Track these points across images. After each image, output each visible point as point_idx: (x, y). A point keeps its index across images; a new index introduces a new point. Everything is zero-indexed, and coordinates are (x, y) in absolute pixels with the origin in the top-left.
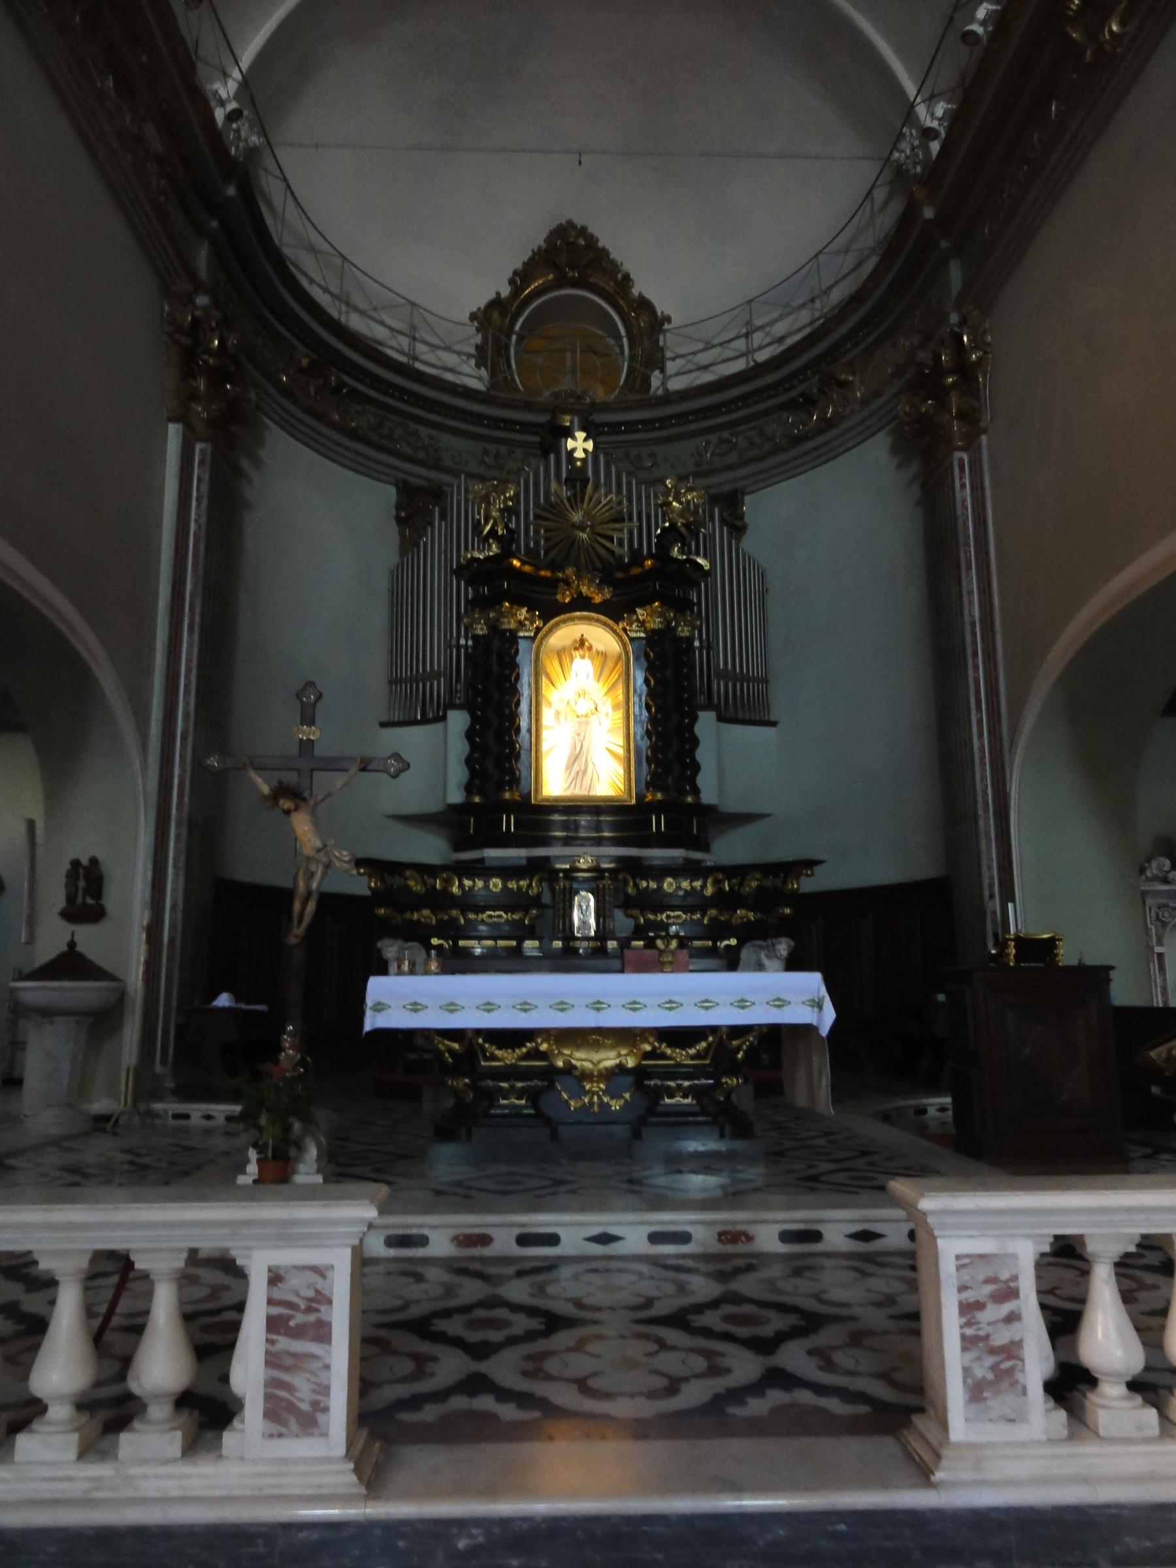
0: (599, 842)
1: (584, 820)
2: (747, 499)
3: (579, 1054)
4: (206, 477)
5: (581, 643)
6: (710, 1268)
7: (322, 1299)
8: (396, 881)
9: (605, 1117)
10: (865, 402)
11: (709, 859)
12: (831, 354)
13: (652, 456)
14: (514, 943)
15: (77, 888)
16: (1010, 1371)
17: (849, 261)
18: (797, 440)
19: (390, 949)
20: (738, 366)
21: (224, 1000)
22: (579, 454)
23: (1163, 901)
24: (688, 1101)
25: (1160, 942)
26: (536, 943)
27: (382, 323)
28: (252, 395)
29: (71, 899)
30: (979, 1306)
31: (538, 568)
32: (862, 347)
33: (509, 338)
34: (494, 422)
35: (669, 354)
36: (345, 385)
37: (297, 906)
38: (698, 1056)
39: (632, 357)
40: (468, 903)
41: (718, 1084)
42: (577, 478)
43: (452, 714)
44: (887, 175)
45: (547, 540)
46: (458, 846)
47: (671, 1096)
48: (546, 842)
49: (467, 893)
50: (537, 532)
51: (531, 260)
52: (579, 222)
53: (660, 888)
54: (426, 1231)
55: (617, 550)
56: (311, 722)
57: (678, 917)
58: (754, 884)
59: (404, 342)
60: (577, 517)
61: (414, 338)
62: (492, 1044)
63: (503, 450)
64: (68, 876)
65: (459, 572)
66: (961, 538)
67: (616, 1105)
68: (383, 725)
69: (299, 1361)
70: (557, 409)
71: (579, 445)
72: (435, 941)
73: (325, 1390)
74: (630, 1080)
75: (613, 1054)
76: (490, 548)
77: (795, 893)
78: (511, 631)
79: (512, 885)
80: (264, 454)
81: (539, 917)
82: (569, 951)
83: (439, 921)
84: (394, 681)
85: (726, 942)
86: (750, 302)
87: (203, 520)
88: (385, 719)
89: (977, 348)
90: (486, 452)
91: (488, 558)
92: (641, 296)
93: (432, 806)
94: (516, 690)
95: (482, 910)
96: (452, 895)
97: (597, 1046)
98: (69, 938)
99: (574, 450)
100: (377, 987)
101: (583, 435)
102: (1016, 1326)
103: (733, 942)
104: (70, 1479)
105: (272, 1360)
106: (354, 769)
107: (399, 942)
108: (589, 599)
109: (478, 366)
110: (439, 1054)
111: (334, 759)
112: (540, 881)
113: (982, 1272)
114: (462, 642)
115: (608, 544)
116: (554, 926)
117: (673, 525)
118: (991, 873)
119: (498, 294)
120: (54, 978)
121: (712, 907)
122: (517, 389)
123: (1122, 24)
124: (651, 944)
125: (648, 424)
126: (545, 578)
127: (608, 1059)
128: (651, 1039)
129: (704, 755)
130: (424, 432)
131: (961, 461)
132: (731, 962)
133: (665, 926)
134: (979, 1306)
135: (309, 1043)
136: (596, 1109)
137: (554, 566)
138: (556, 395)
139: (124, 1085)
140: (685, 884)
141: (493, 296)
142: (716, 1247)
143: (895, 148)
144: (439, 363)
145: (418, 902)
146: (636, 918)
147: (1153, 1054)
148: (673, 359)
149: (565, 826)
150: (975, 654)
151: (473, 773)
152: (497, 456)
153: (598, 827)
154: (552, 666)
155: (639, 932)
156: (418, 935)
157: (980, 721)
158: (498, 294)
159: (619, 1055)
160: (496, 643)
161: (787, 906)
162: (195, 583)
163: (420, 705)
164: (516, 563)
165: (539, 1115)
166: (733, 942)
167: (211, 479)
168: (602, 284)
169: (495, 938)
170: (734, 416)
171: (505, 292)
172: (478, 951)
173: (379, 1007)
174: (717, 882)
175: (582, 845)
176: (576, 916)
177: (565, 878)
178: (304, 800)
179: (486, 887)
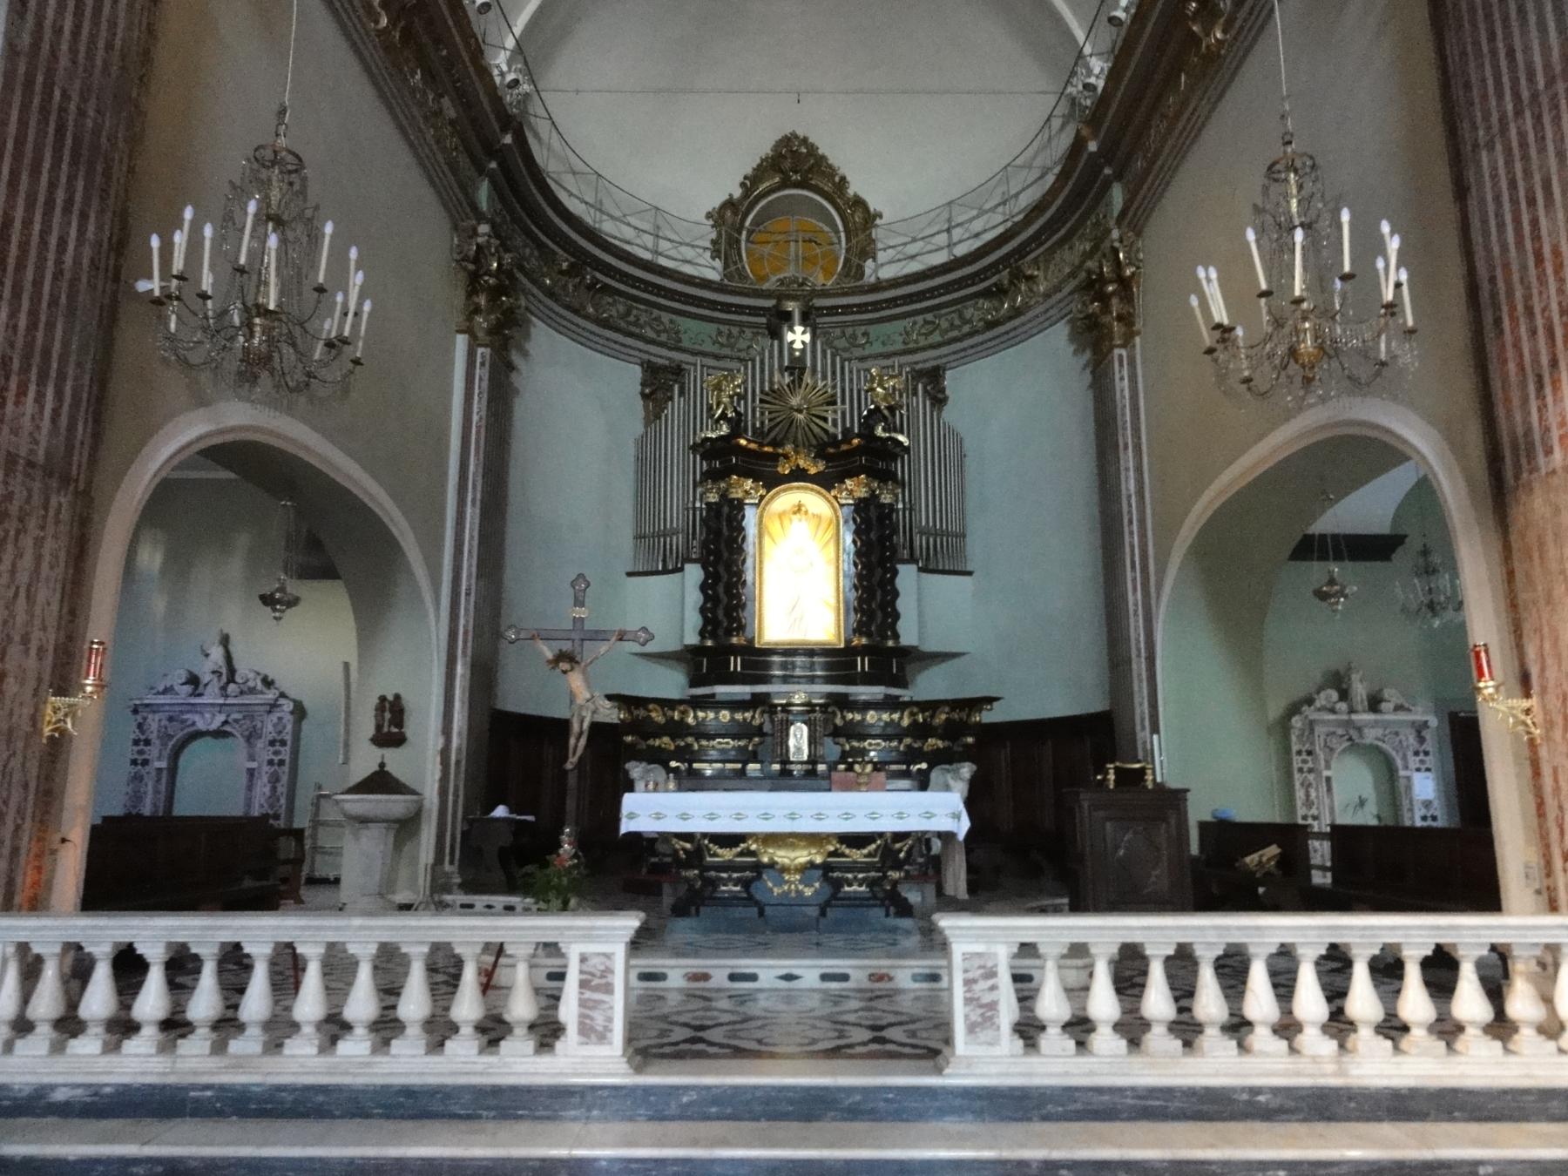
0: (812, 680)
1: (799, 660)
2: (948, 374)
3: (781, 853)
4: (486, 378)
5: (799, 509)
6: (858, 995)
7: (608, 971)
8: (641, 713)
9: (801, 900)
10: (1047, 296)
11: (905, 695)
12: (1021, 251)
13: (865, 334)
14: (739, 766)
15: (383, 719)
16: (991, 1018)
17: (1036, 173)
18: (991, 325)
19: (636, 770)
20: (940, 258)
21: (500, 811)
22: (798, 345)
23: (1332, 729)
24: (863, 888)
25: (1328, 767)
26: (758, 766)
27: (629, 224)
28: (523, 302)
29: (379, 727)
30: (974, 981)
31: (761, 445)
32: (1046, 246)
33: (740, 234)
34: (727, 308)
35: (880, 246)
36: (598, 281)
37: (572, 741)
38: (869, 855)
39: (847, 251)
40: (701, 733)
41: (885, 877)
42: (796, 367)
43: (688, 567)
44: (1063, 108)
45: (770, 420)
46: (694, 683)
47: (850, 885)
48: (765, 680)
49: (701, 723)
50: (762, 414)
51: (760, 166)
52: (801, 133)
53: (864, 719)
54: (664, 970)
55: (831, 430)
56: (582, 605)
57: (878, 744)
58: (943, 717)
59: (648, 240)
60: (795, 401)
61: (657, 236)
62: (715, 844)
63: (735, 330)
64: (376, 710)
65: (694, 448)
66: (1120, 423)
67: (808, 892)
68: (630, 574)
69: (596, 1005)
70: (781, 297)
71: (798, 337)
72: (673, 764)
73: (610, 1020)
74: (820, 872)
75: (805, 853)
76: (721, 430)
77: (980, 725)
78: (738, 499)
79: (739, 716)
80: (530, 347)
81: (761, 743)
82: (785, 773)
83: (677, 747)
84: (639, 537)
85: (918, 766)
86: (950, 203)
87: (484, 413)
88: (630, 569)
89: (1131, 264)
90: (720, 333)
91: (721, 438)
92: (856, 195)
93: (673, 646)
94: (743, 550)
95: (713, 737)
96: (688, 726)
97: (793, 847)
98: (379, 761)
99: (792, 342)
100: (629, 801)
101: (802, 329)
102: (995, 992)
103: (924, 766)
104: (475, 1063)
105: (583, 1003)
106: (614, 639)
107: (644, 764)
108: (805, 470)
109: (713, 258)
110: (676, 851)
111: (597, 632)
112: (763, 713)
113: (977, 963)
114: (698, 505)
115: (821, 423)
116: (773, 751)
117: (877, 409)
118: (1142, 708)
119: (731, 195)
121: (907, 736)
122: (747, 277)
123: (1225, 32)
124: (850, 768)
125: (862, 308)
126: (767, 453)
127: (802, 856)
128: (834, 842)
129: (905, 605)
130: (666, 317)
131: (1121, 356)
132: (923, 785)
133: (864, 752)
134: (974, 981)
135: (581, 843)
136: (793, 895)
137: (776, 443)
138: (782, 282)
139: (423, 880)
140: (885, 717)
141: (727, 197)
142: (867, 984)
143: (1068, 82)
144: (680, 257)
145: (659, 731)
146: (842, 745)
147: (1248, 859)
148: (885, 250)
149: (784, 666)
150: (1131, 522)
151: (706, 621)
153: (812, 667)
154: (773, 526)
155: (844, 756)
156: (658, 758)
157: (1134, 580)
158: (731, 195)
159: (810, 854)
160: (726, 509)
161: (971, 735)
162: (476, 466)
163: (661, 558)
164: (743, 442)
165: (750, 900)
166: (924, 766)
167: (490, 379)
168: (821, 185)
169: (723, 762)
170: (937, 301)
171: (737, 193)
172: (709, 773)
173: (631, 816)
174: (912, 714)
175: (799, 683)
176: (792, 742)
177: (782, 711)
178: (577, 662)
179: (716, 718)
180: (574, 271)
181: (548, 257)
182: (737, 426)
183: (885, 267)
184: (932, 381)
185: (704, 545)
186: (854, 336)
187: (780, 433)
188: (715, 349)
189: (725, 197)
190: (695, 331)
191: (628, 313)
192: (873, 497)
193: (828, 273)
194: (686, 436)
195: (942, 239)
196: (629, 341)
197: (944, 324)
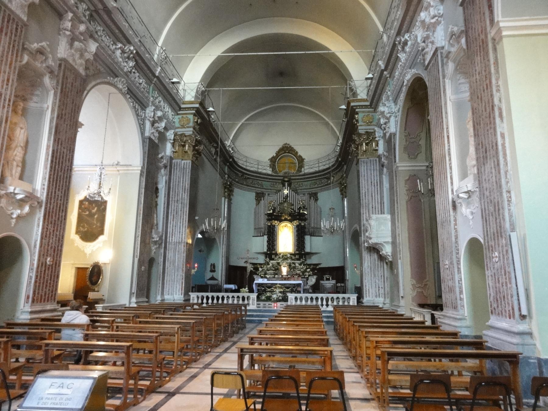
2: (319, 194)
13: (302, 184)
20: (317, 169)
22: (286, 190)
29: (211, 269)
63: (275, 183)
68: (253, 236)
84: (255, 229)
93: (262, 252)
120: (211, 280)
130: (260, 182)
152: (273, 184)
171: (275, 155)
180: (242, 176)
181: (237, 175)
182: (274, 211)
183: (306, 170)
184: (314, 196)
185: (268, 232)
186: (300, 184)
187: (282, 212)
188: (271, 188)
189: (272, 156)
190: (266, 184)
191: (252, 182)
192: (300, 224)
193: (294, 170)
194: (264, 212)
195: (317, 165)
196: (253, 188)
197: (318, 183)
